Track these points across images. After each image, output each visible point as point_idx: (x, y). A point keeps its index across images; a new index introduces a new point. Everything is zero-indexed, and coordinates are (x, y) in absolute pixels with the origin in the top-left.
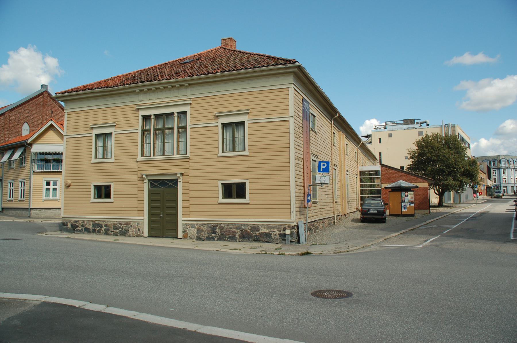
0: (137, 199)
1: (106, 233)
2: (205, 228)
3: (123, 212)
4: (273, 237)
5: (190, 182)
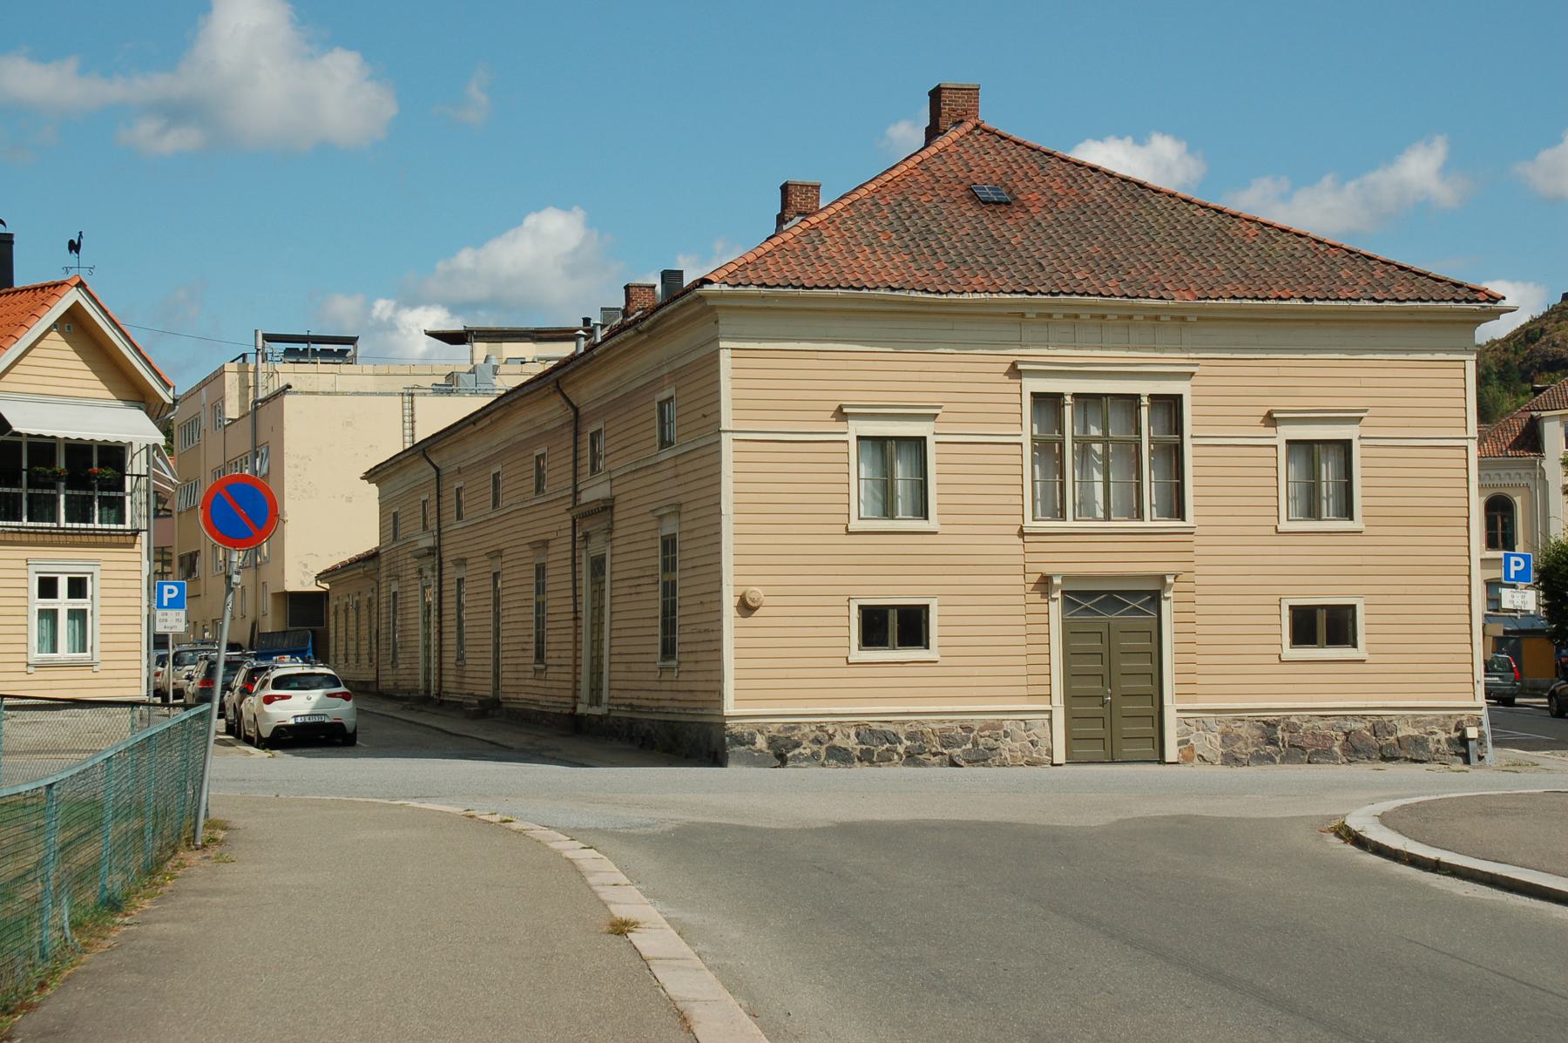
0: (1023, 650)
1: (912, 758)
2: (1244, 730)
3: (975, 691)
4: (1432, 747)
5: (1198, 599)
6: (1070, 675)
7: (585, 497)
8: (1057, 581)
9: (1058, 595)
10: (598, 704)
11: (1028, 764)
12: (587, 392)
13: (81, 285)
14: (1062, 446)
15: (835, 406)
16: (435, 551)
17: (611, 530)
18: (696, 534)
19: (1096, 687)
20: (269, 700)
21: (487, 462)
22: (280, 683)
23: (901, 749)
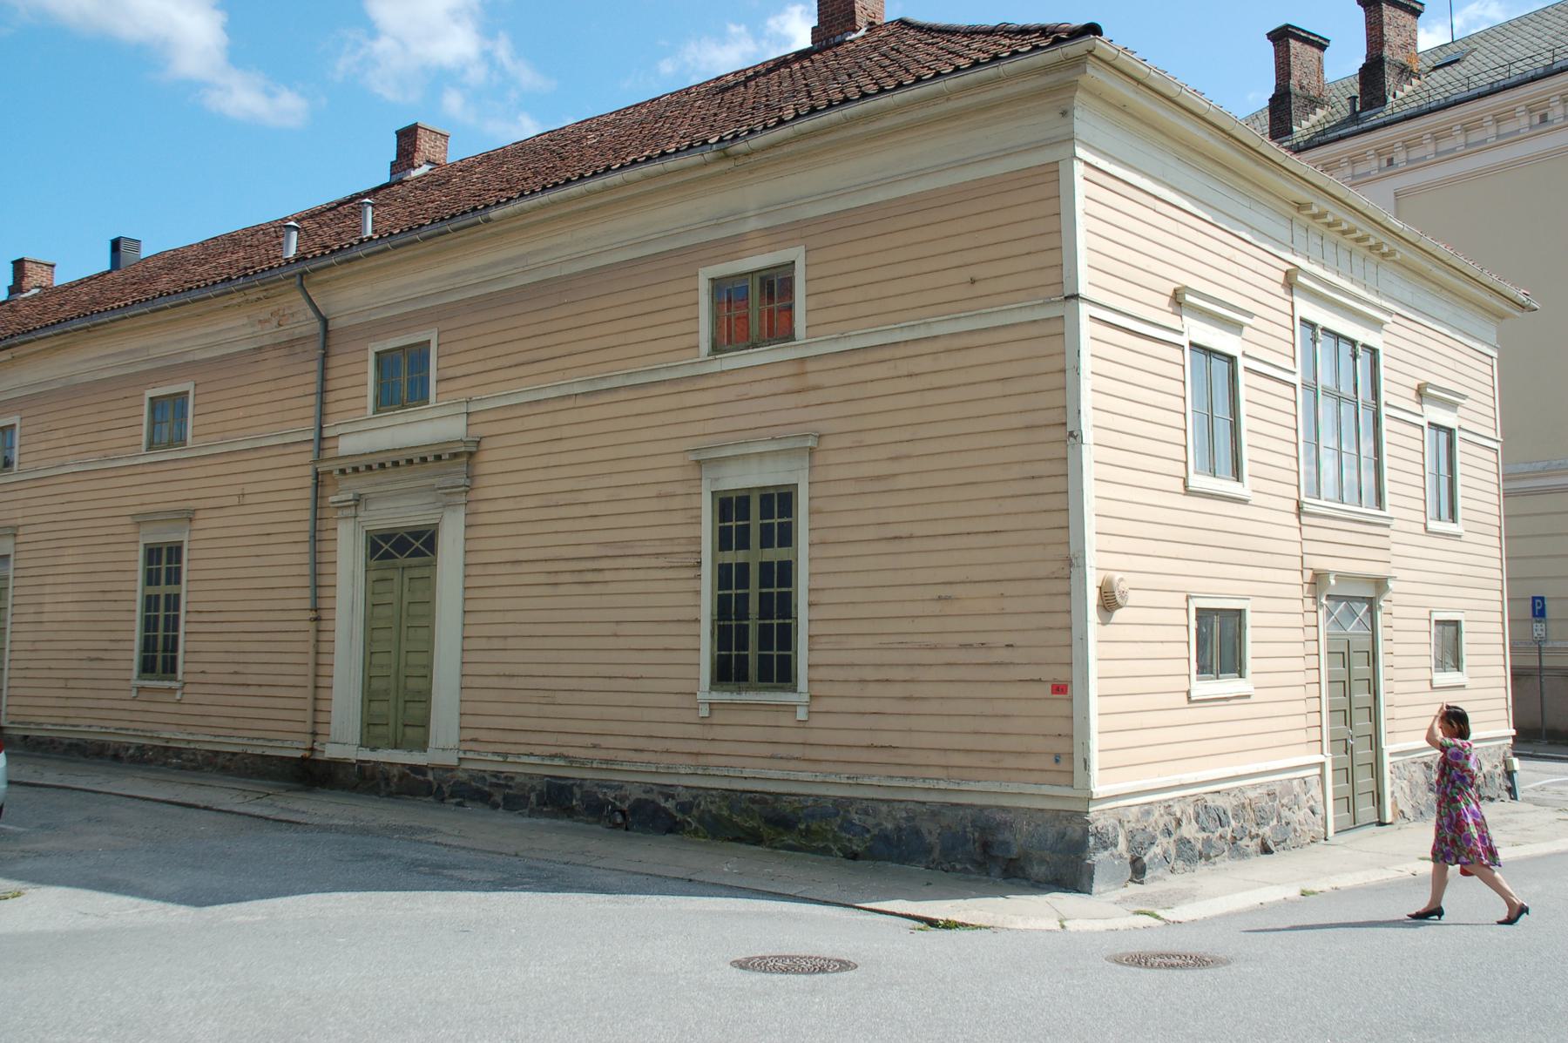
15: (1169, 288)
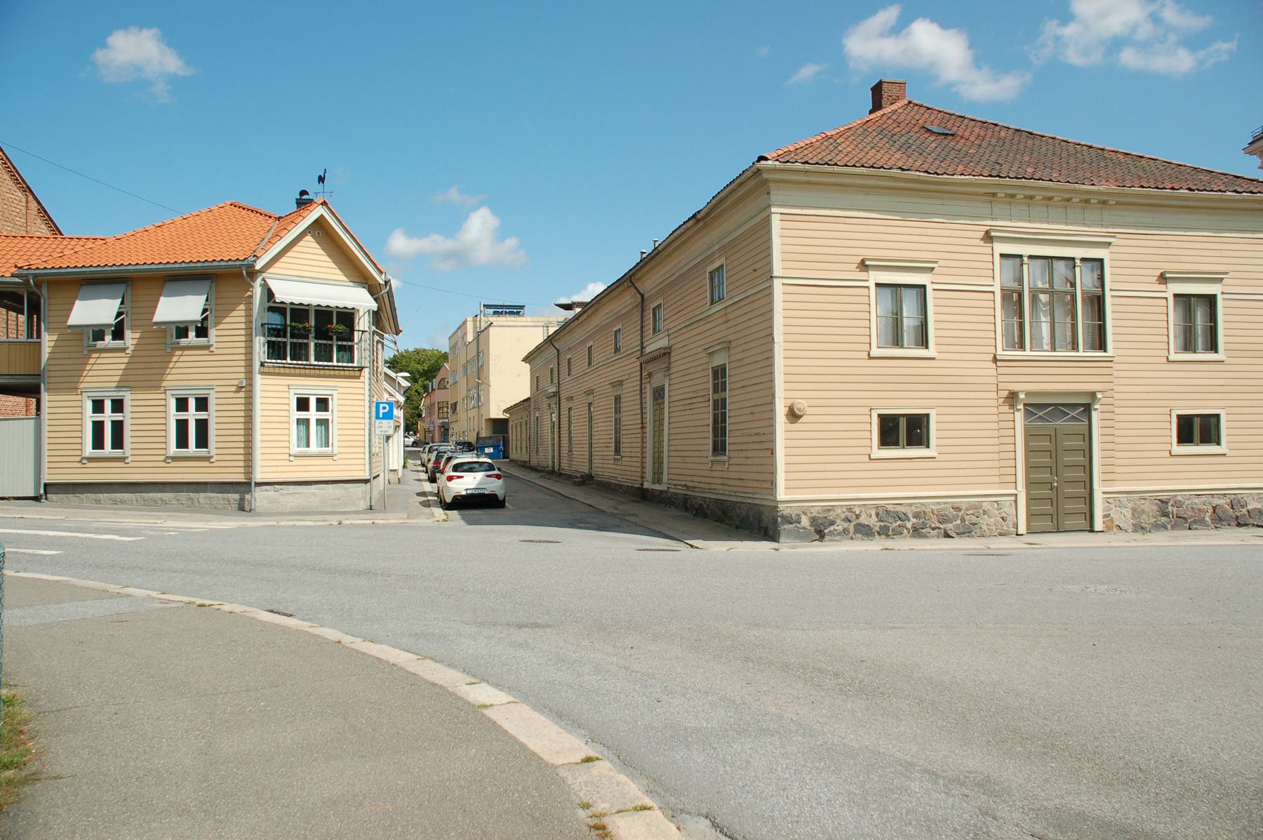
0: (996, 449)
1: (917, 532)
6: (1029, 467)
7: (648, 350)
8: (1022, 396)
9: (1021, 407)
10: (659, 481)
11: (1001, 534)
12: (649, 284)
13: (324, 203)
14: (1020, 295)
15: (859, 260)
16: (557, 394)
17: (669, 369)
18: (745, 362)
19: (1046, 476)
20: (450, 479)
21: (584, 341)
22: (456, 468)
23: (909, 525)
